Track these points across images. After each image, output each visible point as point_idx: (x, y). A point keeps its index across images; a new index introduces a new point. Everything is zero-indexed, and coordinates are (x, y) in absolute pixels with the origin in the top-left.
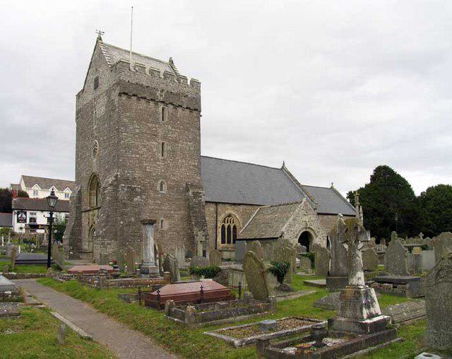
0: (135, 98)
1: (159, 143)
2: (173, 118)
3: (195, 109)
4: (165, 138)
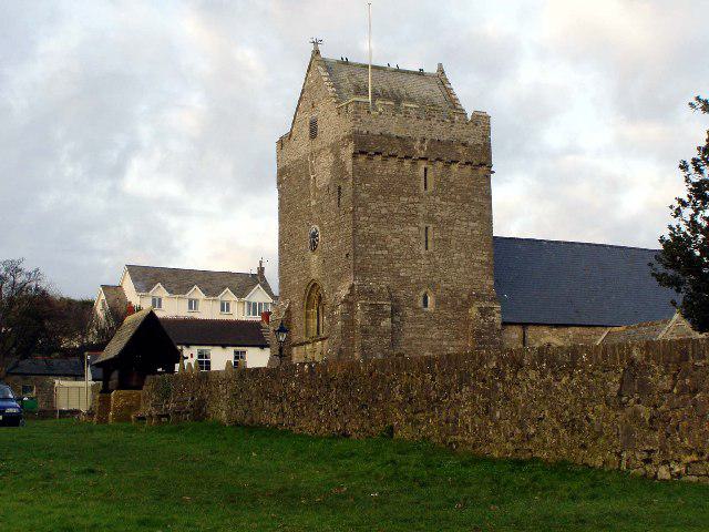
0: (379, 158)
1: (419, 228)
2: (444, 186)
4: (431, 219)
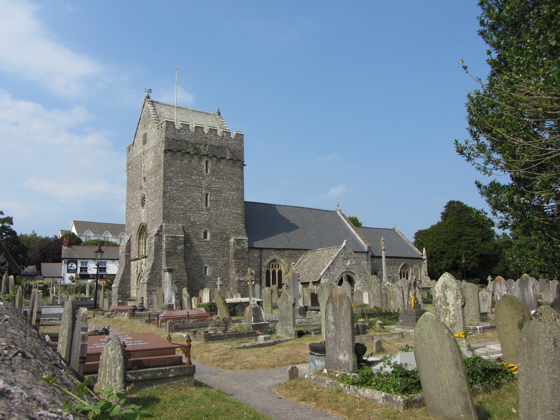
3: (238, 161)
